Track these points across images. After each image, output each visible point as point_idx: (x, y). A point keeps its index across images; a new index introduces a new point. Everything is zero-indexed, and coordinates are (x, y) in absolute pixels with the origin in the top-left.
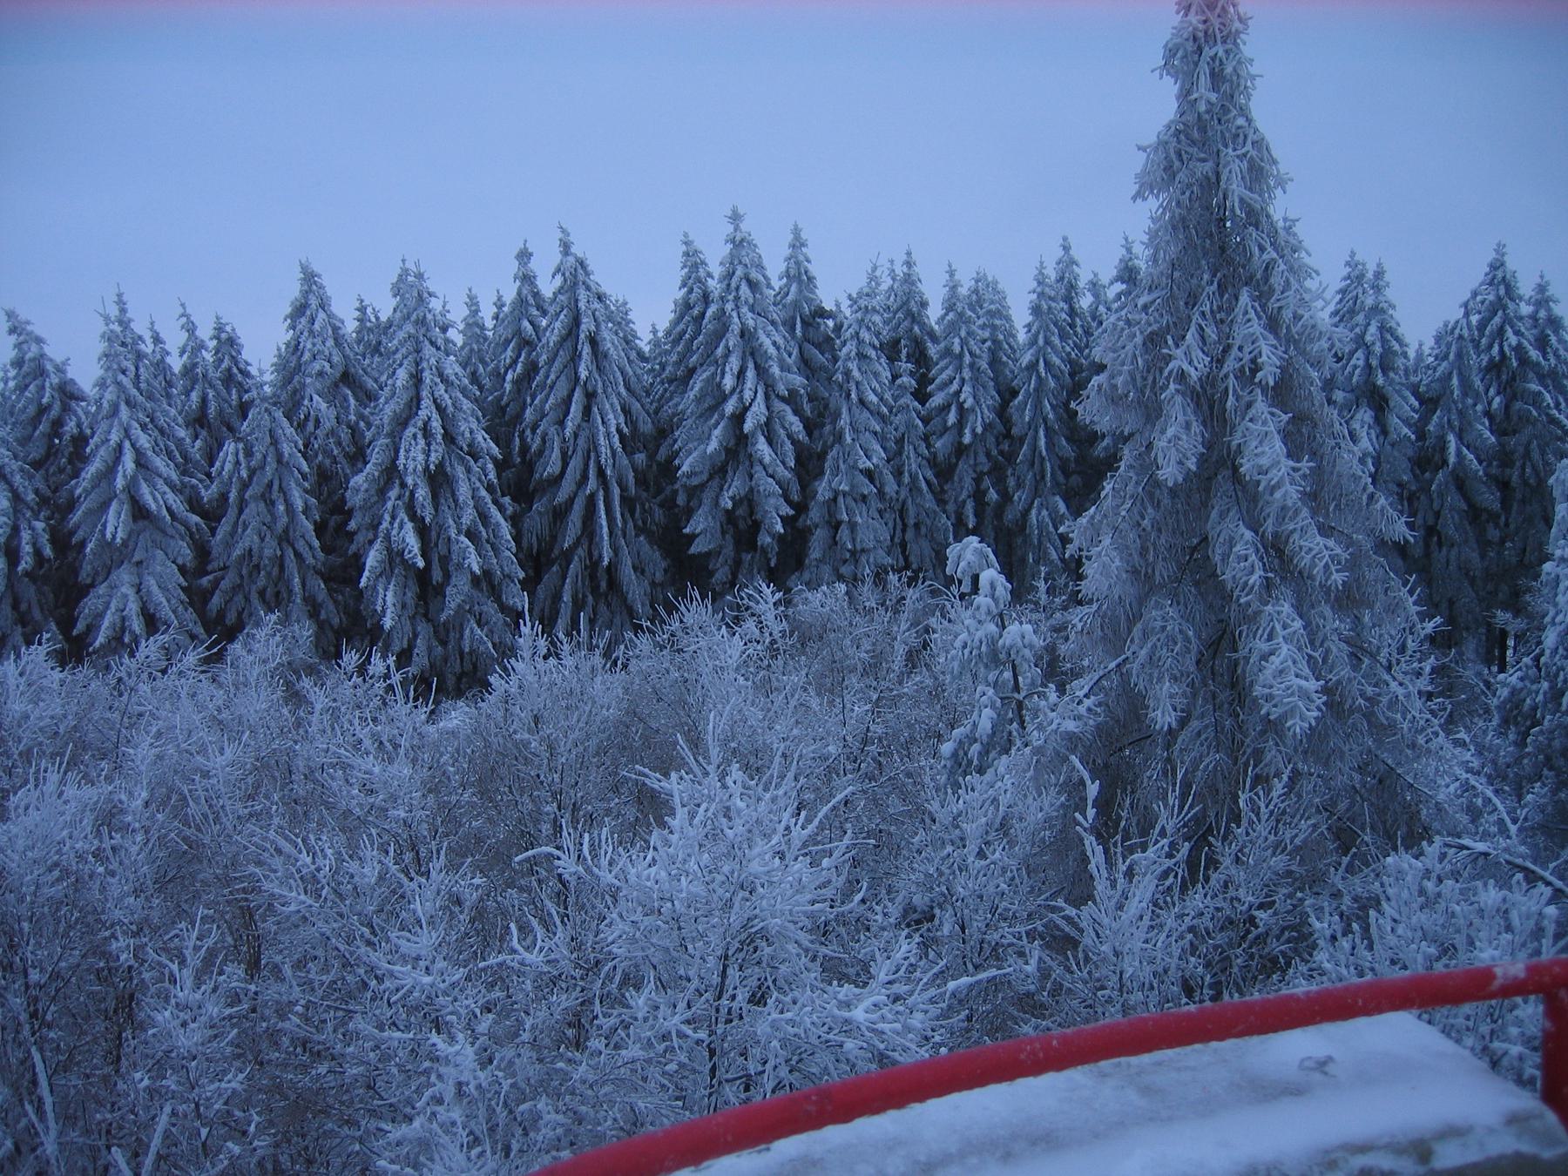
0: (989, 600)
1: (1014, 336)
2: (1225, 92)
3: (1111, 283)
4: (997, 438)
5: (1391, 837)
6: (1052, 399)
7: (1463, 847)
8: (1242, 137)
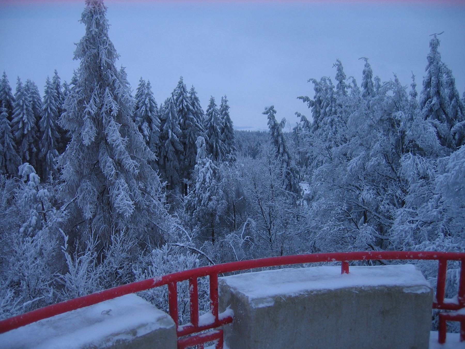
0: (33, 182)
1: (40, 100)
2: (100, 29)
3: (70, 84)
4: (36, 132)
5: (156, 245)
6: (53, 120)
7: (177, 245)
8: (105, 43)
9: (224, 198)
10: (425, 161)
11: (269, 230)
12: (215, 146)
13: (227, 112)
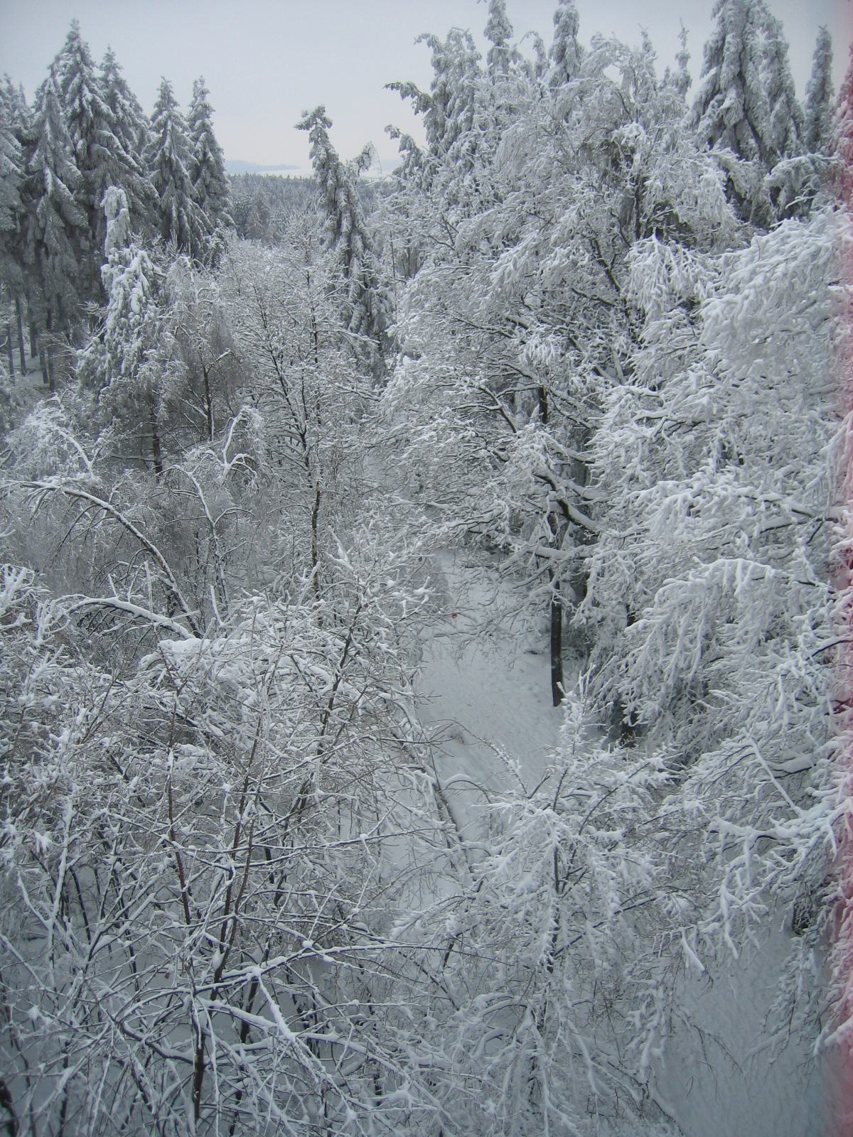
9: (179, 354)
10: (690, 260)
11: (302, 436)
12: (174, 214)
13: (207, 121)
